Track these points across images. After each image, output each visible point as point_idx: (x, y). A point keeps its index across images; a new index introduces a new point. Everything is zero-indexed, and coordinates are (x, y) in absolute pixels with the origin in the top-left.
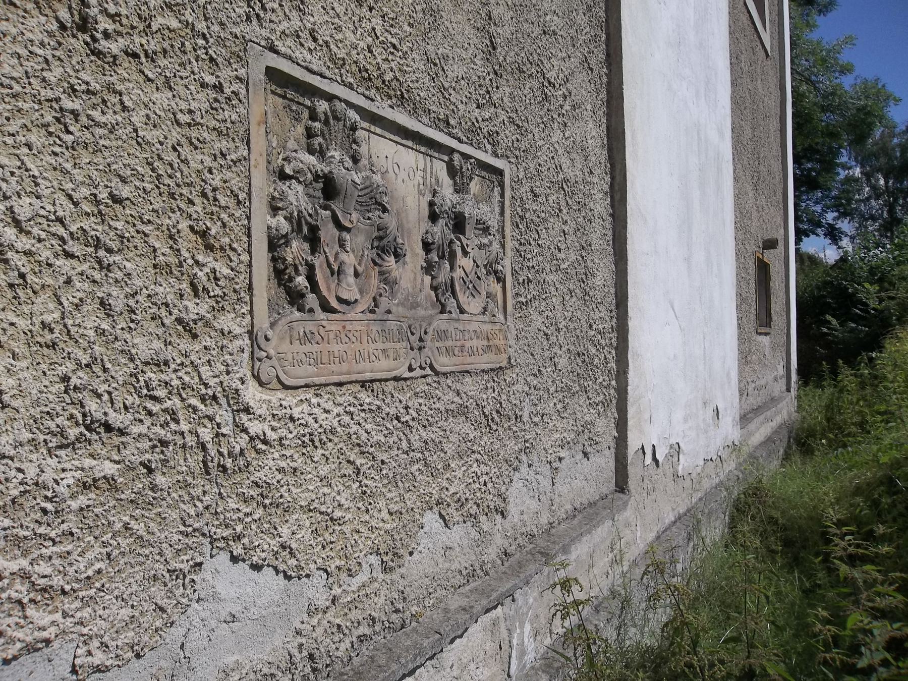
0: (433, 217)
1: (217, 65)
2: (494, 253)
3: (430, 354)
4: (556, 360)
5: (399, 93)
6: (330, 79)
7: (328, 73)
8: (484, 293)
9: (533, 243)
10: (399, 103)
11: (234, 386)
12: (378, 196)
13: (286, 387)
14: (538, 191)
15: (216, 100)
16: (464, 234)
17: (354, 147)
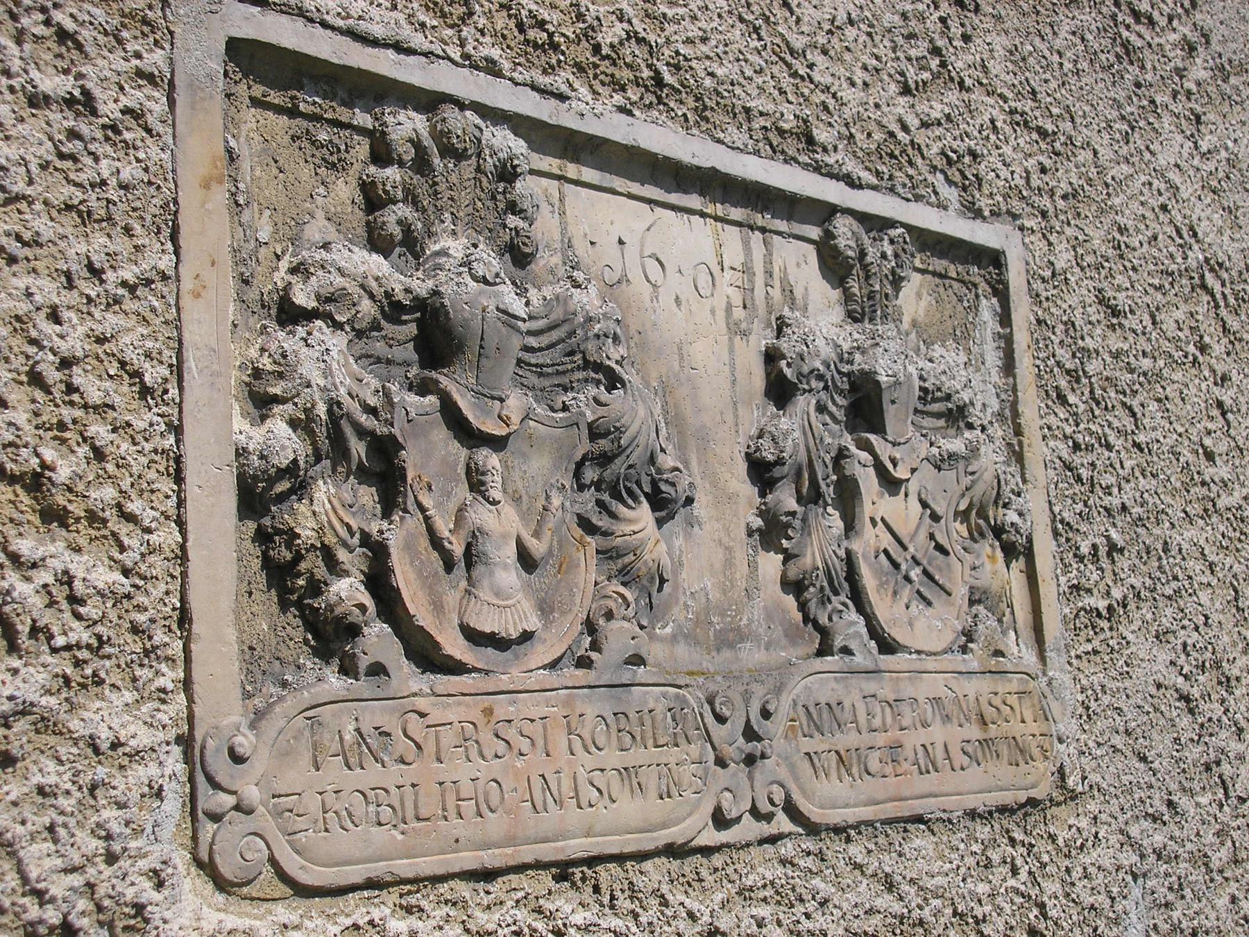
0: (780, 391)
1: (79, 47)
2: (988, 476)
3: (783, 773)
4: (1226, 769)
5: (646, 73)
6: (426, 54)
7: (418, 41)
8: (961, 592)
9: (1118, 443)
10: (650, 98)
11: (130, 893)
12: (591, 346)
13: (304, 891)
14: (1121, 300)
15: (73, 134)
16: (880, 429)
17: (513, 221)
